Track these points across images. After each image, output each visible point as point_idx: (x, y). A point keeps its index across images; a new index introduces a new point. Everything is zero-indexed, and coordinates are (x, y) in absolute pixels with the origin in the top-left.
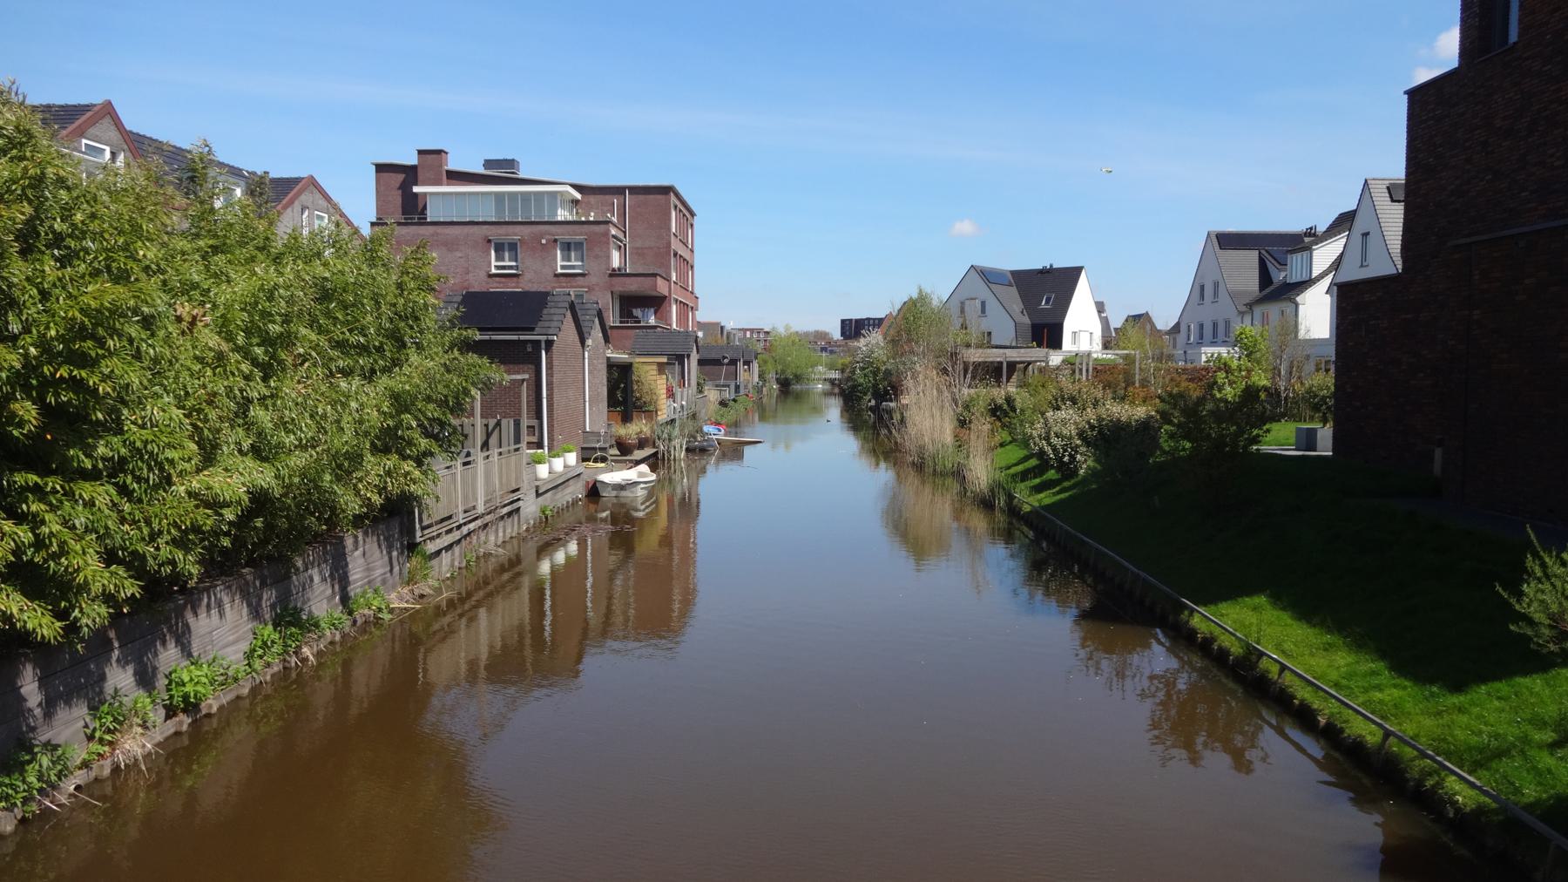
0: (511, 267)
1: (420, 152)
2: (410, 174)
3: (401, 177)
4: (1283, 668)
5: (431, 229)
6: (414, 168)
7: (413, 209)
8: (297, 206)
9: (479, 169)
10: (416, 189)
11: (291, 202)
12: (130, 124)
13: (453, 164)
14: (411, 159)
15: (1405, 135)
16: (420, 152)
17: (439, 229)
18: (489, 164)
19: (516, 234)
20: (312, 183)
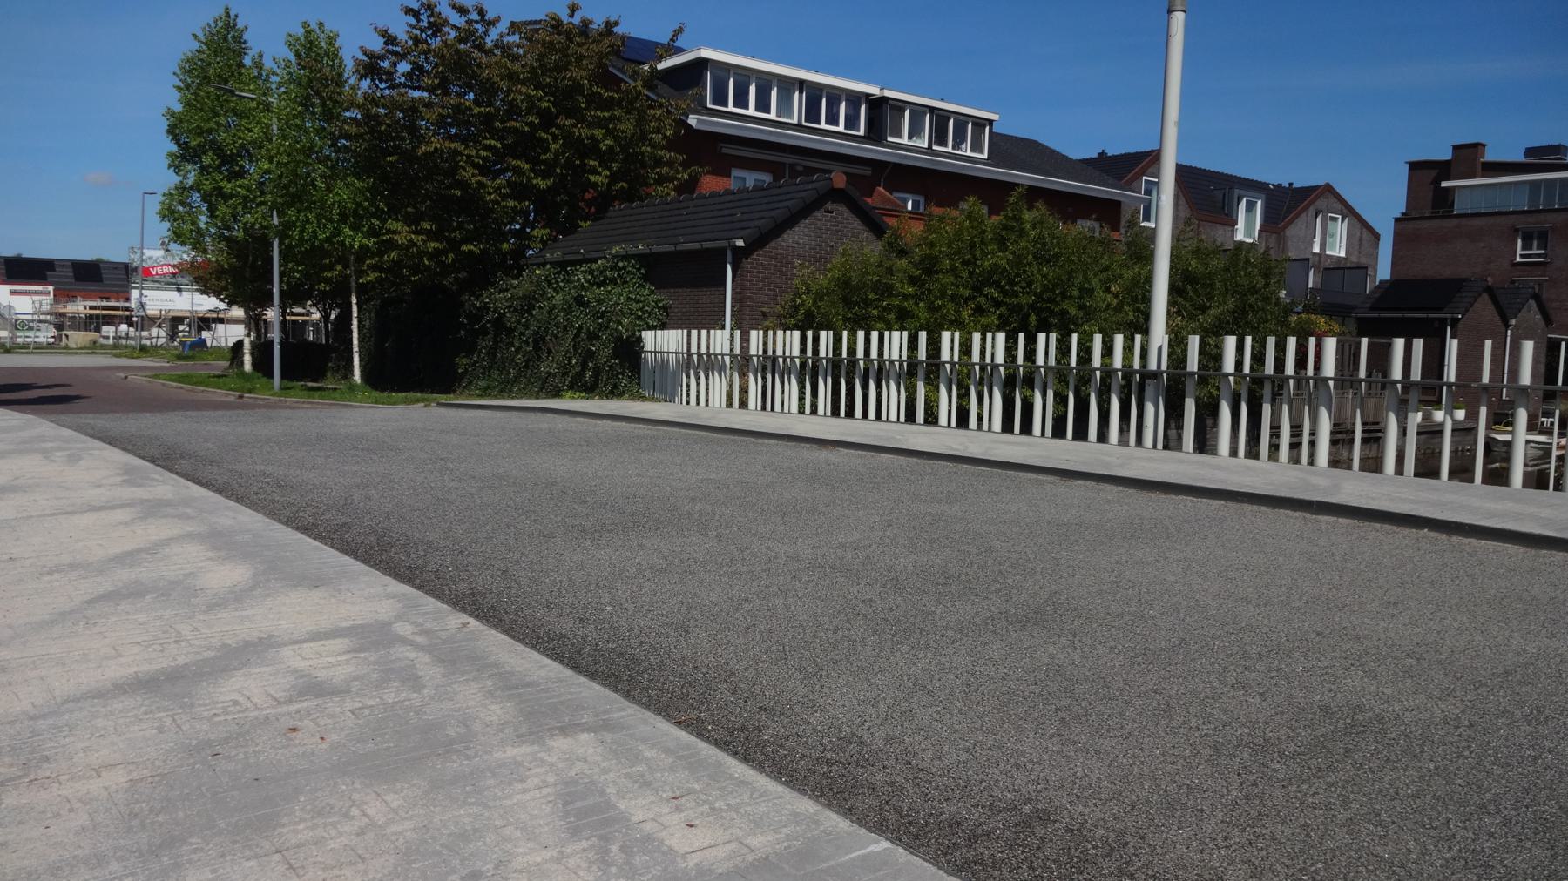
0: (1539, 256)
1: (1456, 148)
2: (1443, 169)
3: (1434, 173)
4: (881, 114)
5: (1455, 222)
6: (1447, 163)
7: (1444, 200)
8: (1312, 211)
9: (1519, 157)
10: (1444, 184)
11: (1307, 207)
12: (1077, 153)
13: (1490, 156)
14: (1446, 155)
15: (1058, 149)
16: (1456, 148)
17: (1464, 221)
18: (1530, 152)
19: (1547, 223)
20: (1328, 189)
